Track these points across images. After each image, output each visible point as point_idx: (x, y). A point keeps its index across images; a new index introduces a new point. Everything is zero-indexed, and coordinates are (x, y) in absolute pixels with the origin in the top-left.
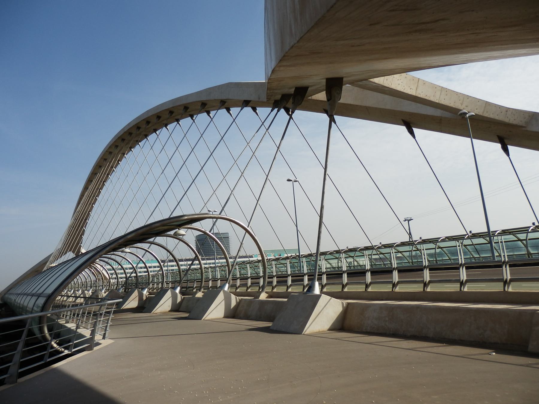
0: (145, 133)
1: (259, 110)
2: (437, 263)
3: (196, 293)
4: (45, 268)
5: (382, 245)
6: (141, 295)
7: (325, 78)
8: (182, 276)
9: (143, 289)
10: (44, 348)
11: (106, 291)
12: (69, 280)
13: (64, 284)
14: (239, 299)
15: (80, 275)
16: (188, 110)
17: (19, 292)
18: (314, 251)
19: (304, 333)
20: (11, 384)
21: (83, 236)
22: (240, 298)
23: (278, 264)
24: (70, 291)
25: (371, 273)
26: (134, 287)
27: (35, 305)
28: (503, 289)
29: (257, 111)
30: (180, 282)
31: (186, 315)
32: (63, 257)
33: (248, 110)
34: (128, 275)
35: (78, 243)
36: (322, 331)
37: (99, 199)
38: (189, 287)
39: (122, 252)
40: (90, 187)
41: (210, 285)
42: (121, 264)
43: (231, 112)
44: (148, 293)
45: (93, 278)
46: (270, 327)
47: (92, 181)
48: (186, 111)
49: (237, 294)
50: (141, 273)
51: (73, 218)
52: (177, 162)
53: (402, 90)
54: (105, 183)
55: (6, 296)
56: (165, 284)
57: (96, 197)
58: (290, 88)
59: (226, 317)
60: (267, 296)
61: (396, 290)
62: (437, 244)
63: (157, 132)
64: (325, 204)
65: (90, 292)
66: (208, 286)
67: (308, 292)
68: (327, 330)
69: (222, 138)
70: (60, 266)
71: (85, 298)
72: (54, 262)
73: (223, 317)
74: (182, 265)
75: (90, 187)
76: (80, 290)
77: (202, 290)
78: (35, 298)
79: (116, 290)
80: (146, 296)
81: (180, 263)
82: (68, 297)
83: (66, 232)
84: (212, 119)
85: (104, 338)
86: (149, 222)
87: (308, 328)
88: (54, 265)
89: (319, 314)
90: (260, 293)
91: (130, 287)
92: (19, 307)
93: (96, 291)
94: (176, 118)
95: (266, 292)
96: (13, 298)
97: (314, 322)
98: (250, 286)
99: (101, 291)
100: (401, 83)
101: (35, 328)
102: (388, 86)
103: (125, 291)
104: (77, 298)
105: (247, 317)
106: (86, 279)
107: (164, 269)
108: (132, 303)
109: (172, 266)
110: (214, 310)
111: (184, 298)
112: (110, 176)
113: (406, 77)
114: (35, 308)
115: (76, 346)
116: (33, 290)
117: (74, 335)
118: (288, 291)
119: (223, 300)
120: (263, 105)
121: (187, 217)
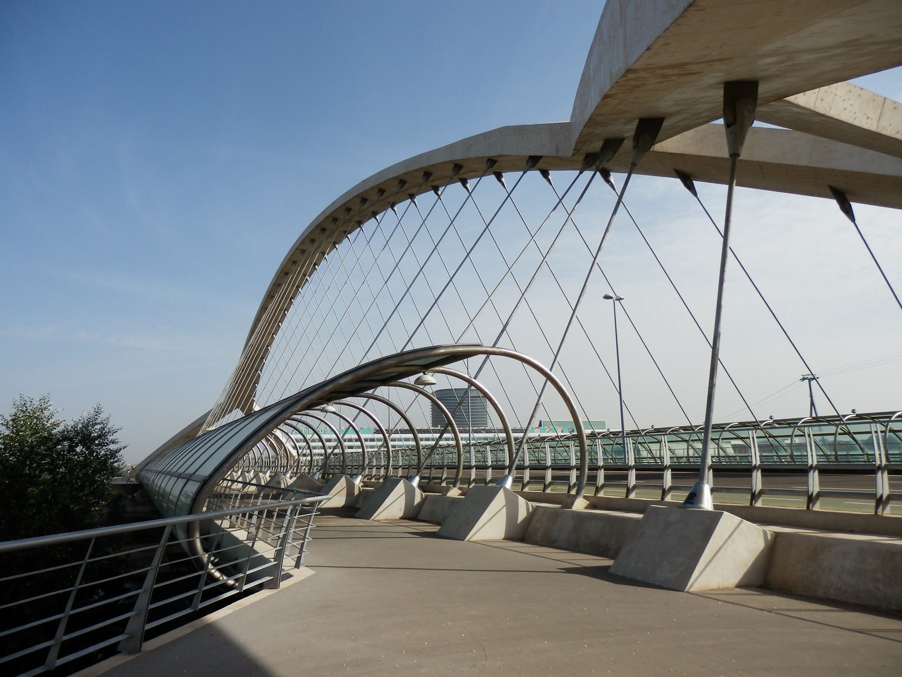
0: (358, 219)
1: (553, 174)
2: (836, 458)
3: (448, 489)
4: (200, 433)
5: (774, 421)
6: (350, 486)
7: (719, 83)
8: (423, 458)
9: (353, 476)
10: (193, 584)
11: (291, 475)
12: (239, 454)
13: (231, 461)
14: (532, 506)
15: (258, 445)
16: (431, 179)
17: (160, 469)
18: (699, 420)
19: (688, 590)
20: (129, 653)
21: (256, 385)
22: (535, 504)
23: (558, 447)
24: (236, 472)
25: (713, 472)
26: (337, 471)
27: (183, 493)
28: (874, 511)
29: (550, 177)
30: (418, 468)
31: (436, 529)
32: (227, 417)
33: (535, 175)
34: (329, 451)
35: (249, 396)
36: (725, 588)
37: (283, 326)
38: (434, 478)
39: (323, 410)
40: (270, 305)
41: (473, 477)
42: (317, 431)
43: (503, 180)
44: (362, 484)
45: (272, 453)
46: (608, 567)
47: (273, 297)
48: (427, 180)
49: (529, 498)
50: (352, 448)
51: (243, 356)
52: (409, 267)
53: (850, 120)
54: (293, 300)
55: (143, 473)
56: (391, 469)
57: (278, 324)
58: (629, 121)
59: (509, 538)
60: (586, 505)
61: (885, 512)
62: (888, 425)
63: (378, 217)
64: (722, 329)
65: (268, 474)
66: (469, 477)
67: (689, 505)
68: (733, 586)
69: (487, 226)
70: (223, 429)
71: (258, 485)
72: (213, 424)
73: (504, 539)
74: (422, 440)
75: (269, 307)
76: (251, 471)
77: (458, 485)
78: (183, 481)
79: (308, 475)
80: (359, 487)
81: (420, 436)
82: (245, 484)
83: (232, 377)
84: (470, 194)
85: (297, 566)
86: (374, 356)
87: (697, 579)
88: (214, 428)
89: (717, 552)
90: (574, 497)
91: (332, 471)
92: (158, 494)
93: (276, 474)
94: (411, 191)
95: (584, 496)
96: (151, 476)
97: (708, 569)
98: (550, 484)
99: (285, 474)
100: (849, 107)
101: (183, 540)
102: (823, 112)
103: (323, 477)
104: (245, 484)
105: (549, 542)
106: (261, 454)
107: (391, 443)
108: (336, 498)
109: (407, 440)
110: (488, 523)
111: (426, 496)
112: (302, 289)
113: (859, 95)
114: (182, 498)
115: (250, 578)
116: (179, 468)
117: (247, 558)
118: (524, 490)
119: (503, 508)
120: (563, 163)
121: (443, 351)
